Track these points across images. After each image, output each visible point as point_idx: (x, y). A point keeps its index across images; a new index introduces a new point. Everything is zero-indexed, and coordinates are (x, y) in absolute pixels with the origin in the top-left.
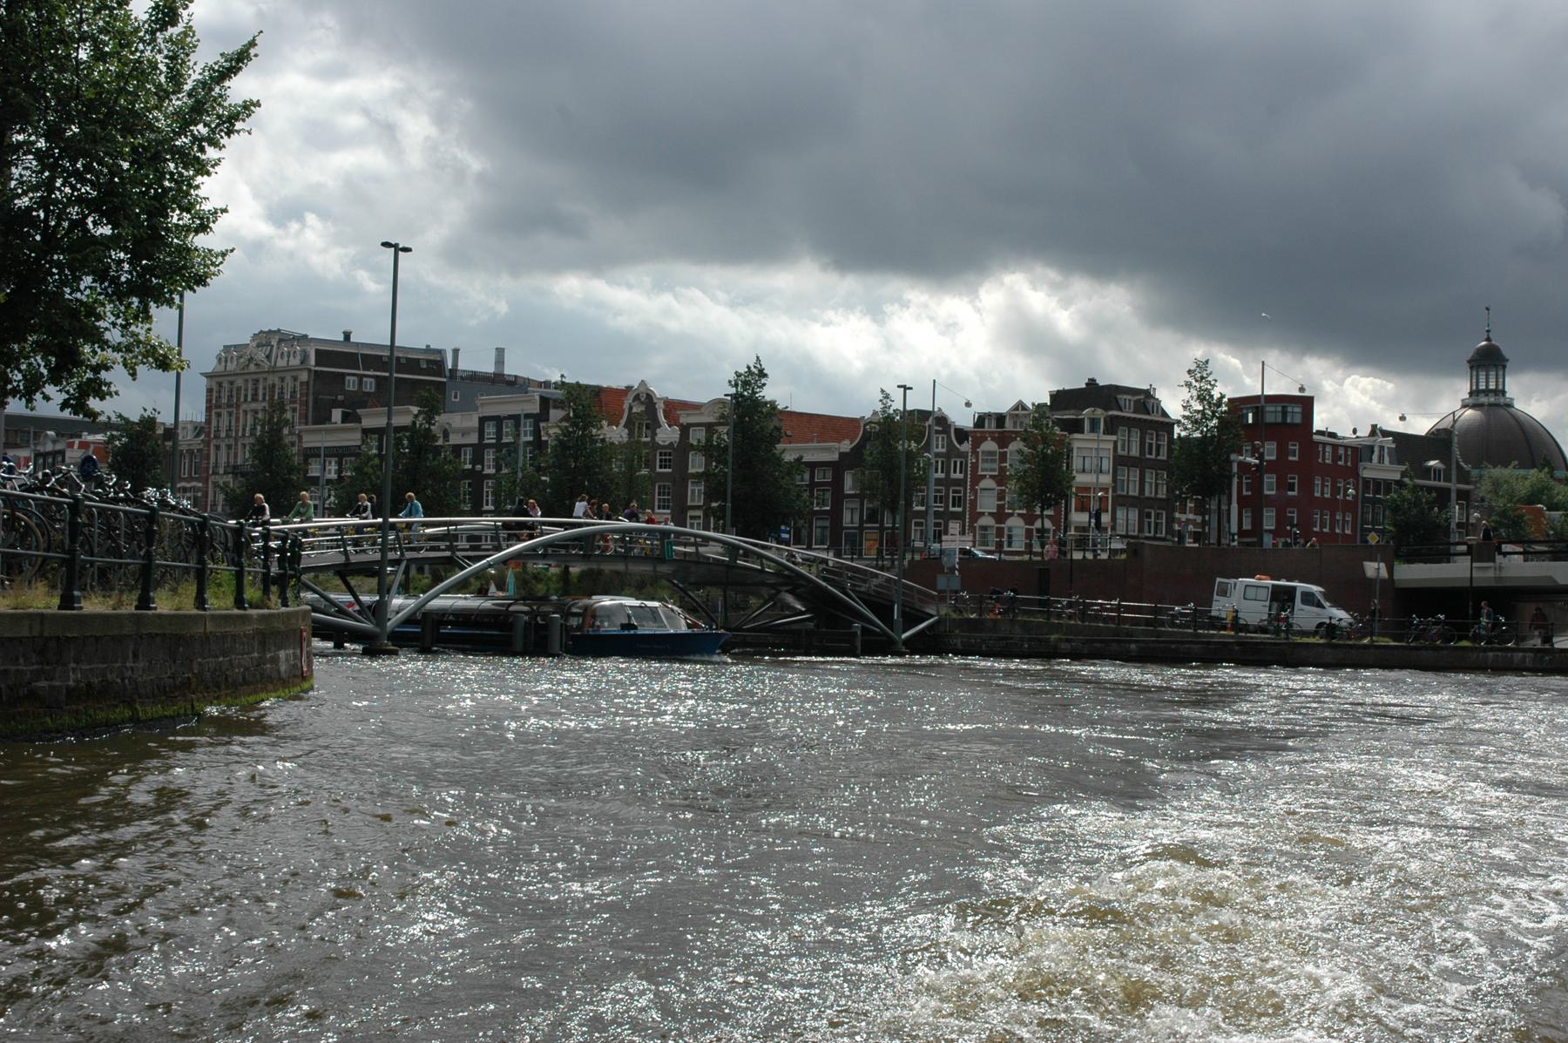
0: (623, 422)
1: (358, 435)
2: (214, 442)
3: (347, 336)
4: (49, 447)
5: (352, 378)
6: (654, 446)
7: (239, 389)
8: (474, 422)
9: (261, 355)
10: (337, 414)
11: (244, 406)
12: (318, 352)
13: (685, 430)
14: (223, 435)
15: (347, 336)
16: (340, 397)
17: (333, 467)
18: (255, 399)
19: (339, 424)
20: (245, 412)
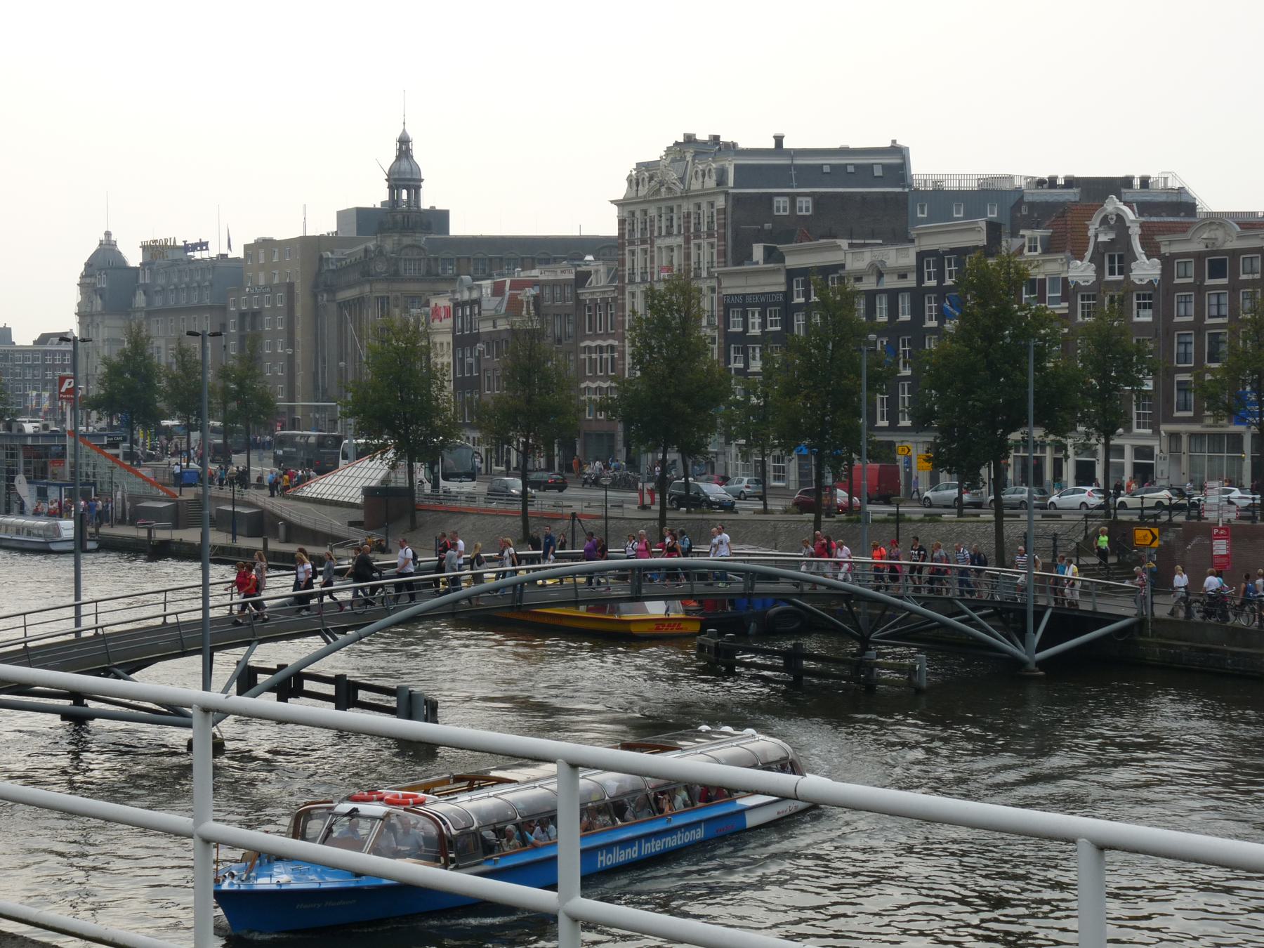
0: (1088, 254)
1: (782, 279)
2: (629, 289)
3: (779, 140)
4: (466, 296)
5: (804, 199)
6: (1128, 287)
7: (652, 221)
8: (910, 260)
9: (673, 176)
10: (758, 251)
11: (658, 242)
12: (738, 168)
13: (1167, 262)
14: (638, 279)
15: (779, 140)
16: (768, 226)
17: (756, 320)
18: (669, 234)
19: (762, 265)
20: (660, 248)
